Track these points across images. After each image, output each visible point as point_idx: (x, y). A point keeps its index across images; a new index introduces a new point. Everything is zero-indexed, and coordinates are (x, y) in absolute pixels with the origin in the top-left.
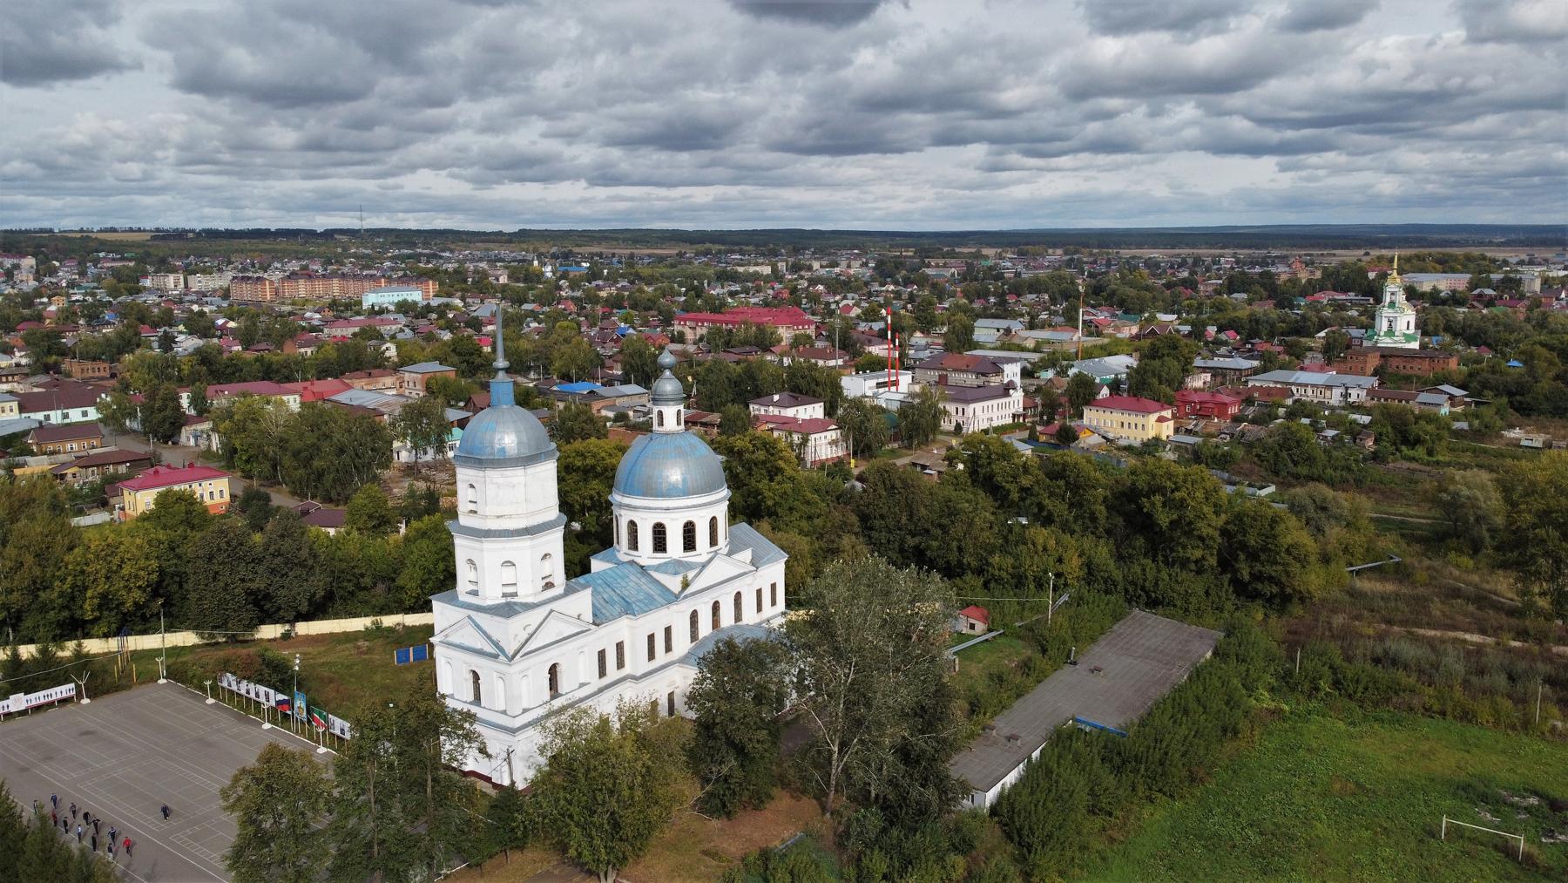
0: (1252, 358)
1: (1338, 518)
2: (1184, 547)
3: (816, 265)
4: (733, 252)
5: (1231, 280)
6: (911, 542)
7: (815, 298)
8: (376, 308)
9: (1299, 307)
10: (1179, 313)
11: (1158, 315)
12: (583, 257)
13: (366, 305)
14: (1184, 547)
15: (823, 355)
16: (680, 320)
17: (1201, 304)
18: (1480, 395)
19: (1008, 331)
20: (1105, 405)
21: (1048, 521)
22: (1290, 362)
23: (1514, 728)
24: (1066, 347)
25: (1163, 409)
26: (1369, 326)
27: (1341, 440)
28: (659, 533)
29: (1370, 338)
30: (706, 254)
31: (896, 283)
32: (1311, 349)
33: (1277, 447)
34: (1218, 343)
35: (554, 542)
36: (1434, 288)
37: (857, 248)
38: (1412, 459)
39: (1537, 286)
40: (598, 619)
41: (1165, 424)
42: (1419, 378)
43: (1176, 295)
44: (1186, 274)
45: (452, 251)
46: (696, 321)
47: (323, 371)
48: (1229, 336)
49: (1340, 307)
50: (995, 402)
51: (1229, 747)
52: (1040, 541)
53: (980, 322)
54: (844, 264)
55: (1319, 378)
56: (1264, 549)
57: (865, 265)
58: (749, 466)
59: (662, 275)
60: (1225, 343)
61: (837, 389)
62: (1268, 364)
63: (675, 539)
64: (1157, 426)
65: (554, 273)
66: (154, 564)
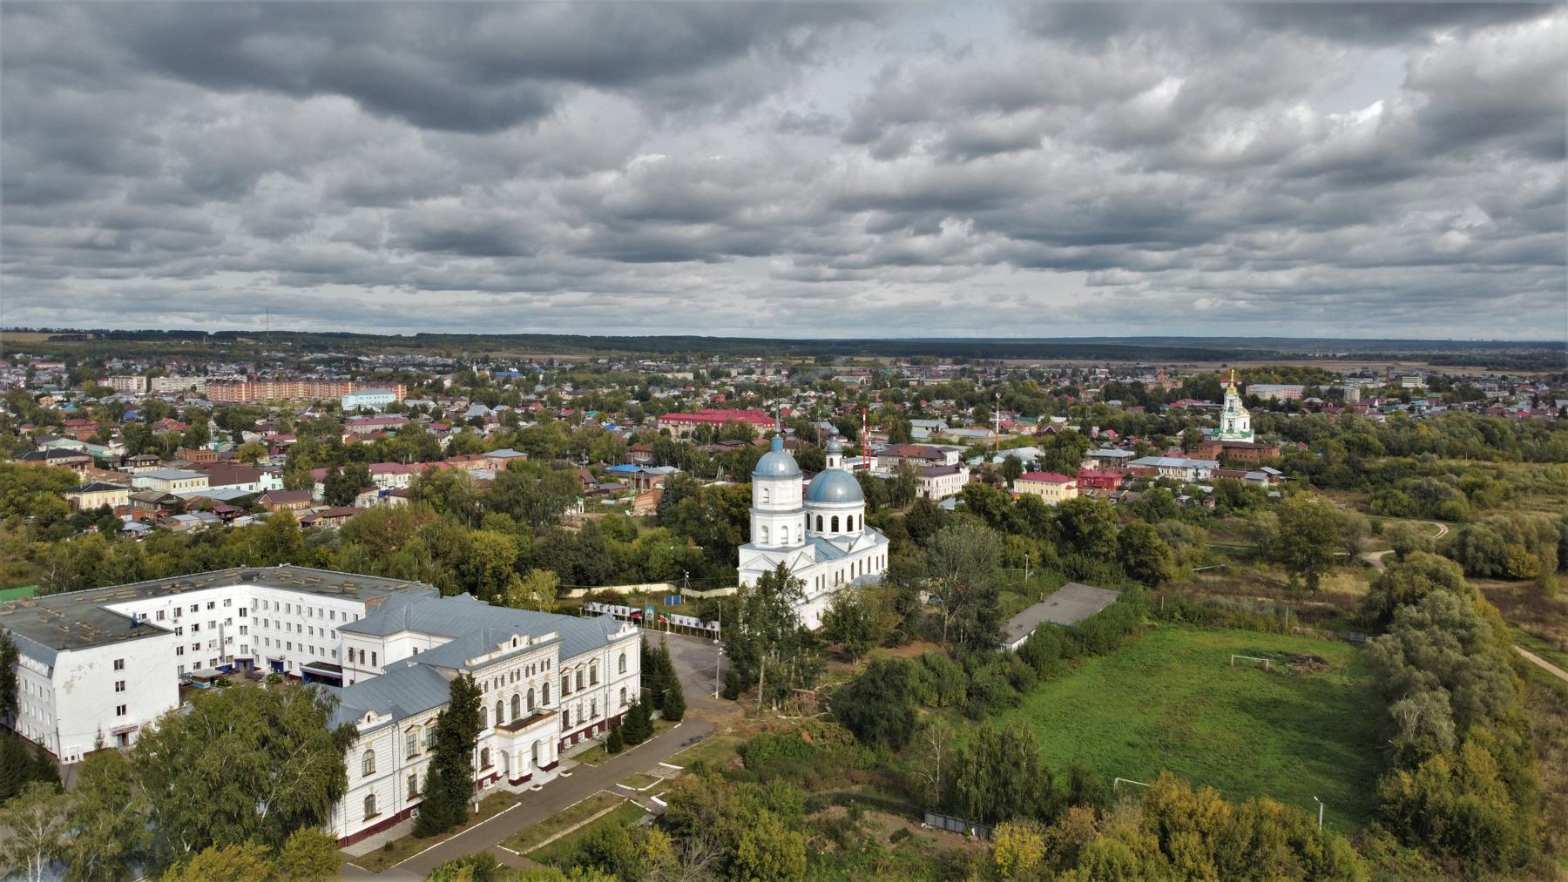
0: (1128, 449)
1: (1187, 541)
3: (734, 372)
5: (1107, 388)
9: (1164, 412)
17: (1083, 410)
18: (1290, 474)
19: (936, 430)
20: (1024, 478)
21: (1017, 532)
26: (1217, 426)
29: (1216, 435)
31: (816, 390)
32: (1173, 444)
34: (1101, 439)
38: (1241, 516)
39: (1357, 396)
43: (1063, 401)
44: (1067, 383)
46: (679, 420)
49: (1196, 411)
51: (1127, 638)
52: (1015, 542)
55: (1178, 462)
56: (1144, 546)
60: (1107, 440)
62: (1141, 452)
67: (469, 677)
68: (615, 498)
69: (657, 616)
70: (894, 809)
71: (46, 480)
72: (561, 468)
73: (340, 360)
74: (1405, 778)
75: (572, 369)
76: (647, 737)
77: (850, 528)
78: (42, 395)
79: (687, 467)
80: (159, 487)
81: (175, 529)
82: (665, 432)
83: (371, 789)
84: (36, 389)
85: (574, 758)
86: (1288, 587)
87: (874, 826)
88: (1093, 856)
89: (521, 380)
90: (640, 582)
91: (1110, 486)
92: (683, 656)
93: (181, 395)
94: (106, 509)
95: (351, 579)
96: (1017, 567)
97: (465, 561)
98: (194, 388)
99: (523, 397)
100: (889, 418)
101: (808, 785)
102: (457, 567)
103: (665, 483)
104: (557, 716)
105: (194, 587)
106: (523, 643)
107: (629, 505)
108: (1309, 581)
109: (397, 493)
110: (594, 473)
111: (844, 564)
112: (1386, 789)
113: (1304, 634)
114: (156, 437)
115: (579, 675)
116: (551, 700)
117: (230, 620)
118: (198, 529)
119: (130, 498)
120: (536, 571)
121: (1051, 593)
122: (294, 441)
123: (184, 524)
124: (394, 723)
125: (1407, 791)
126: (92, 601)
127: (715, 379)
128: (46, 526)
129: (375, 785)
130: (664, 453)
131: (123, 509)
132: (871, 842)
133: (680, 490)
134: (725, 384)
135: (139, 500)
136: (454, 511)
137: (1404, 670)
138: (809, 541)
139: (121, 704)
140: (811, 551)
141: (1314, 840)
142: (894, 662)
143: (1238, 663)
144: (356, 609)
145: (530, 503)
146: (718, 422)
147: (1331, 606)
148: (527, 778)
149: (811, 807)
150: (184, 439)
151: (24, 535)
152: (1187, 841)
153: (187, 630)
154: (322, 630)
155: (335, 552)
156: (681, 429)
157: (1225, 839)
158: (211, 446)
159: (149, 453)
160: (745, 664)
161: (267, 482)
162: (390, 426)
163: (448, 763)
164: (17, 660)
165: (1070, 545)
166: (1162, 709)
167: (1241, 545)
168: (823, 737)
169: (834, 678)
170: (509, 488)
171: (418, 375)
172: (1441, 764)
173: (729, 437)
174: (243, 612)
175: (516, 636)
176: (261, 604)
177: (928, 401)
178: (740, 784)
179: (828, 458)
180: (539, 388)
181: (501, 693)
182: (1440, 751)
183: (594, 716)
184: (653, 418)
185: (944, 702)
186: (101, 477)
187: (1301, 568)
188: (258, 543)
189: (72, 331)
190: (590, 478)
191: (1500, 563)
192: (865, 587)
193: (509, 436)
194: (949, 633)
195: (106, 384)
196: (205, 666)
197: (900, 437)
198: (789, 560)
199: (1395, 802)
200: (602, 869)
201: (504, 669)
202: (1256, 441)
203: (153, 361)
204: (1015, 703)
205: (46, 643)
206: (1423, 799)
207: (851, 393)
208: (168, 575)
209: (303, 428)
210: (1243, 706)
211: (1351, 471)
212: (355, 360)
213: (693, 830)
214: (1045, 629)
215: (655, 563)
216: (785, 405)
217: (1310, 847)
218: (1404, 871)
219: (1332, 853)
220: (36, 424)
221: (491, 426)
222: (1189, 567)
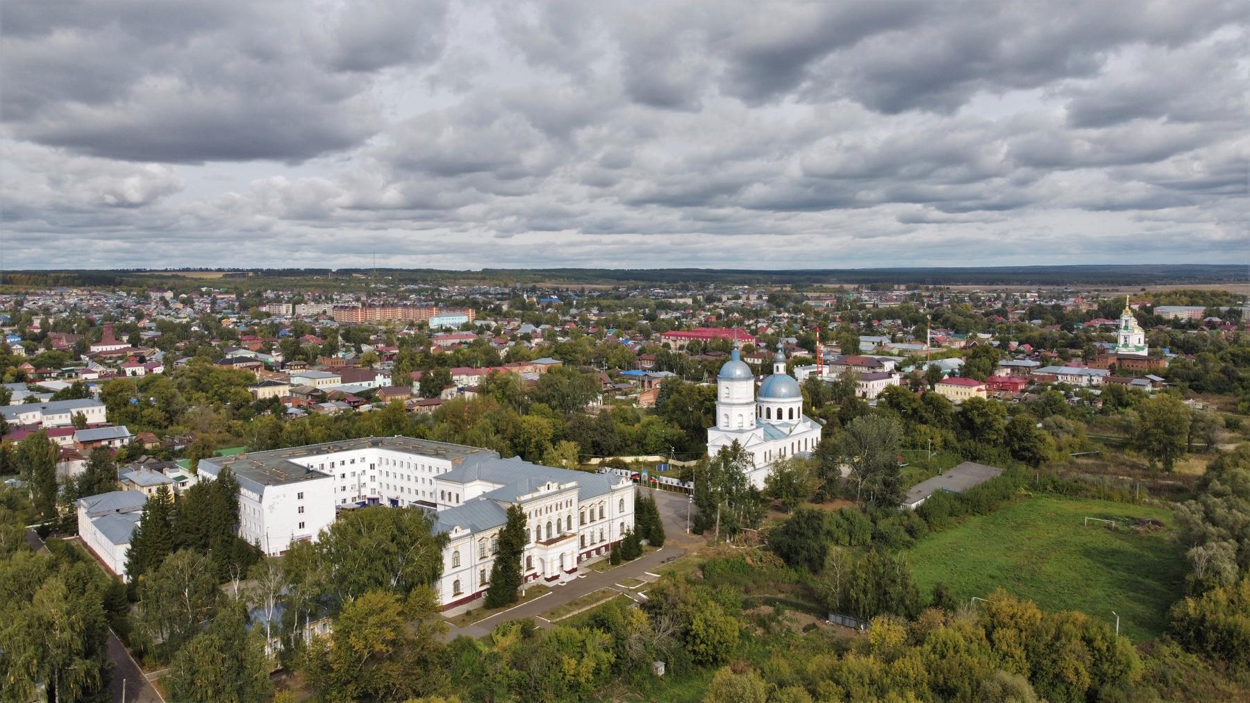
2: (988, 434)
3: (724, 298)
4: (654, 287)
10: (993, 333)
11: (978, 334)
14: (988, 434)
18: (1172, 381)
19: (880, 344)
20: (946, 382)
21: (925, 423)
22: (1058, 362)
23: (1128, 502)
24: (919, 353)
25: (980, 384)
27: (1083, 403)
29: (1113, 348)
31: (788, 312)
33: (1044, 405)
34: (1018, 352)
36: (1176, 316)
37: (746, 284)
42: (1136, 372)
44: (999, 305)
46: (677, 336)
48: (1026, 348)
51: (1005, 503)
56: (1025, 435)
60: (1022, 352)
62: (1045, 362)
64: (978, 392)
67: (519, 507)
68: (626, 394)
69: (650, 478)
70: (808, 610)
71: (236, 379)
72: (587, 372)
73: (426, 290)
74: (1191, 603)
75: (599, 296)
76: (638, 555)
77: (791, 417)
78: (223, 318)
79: (680, 373)
80: (309, 383)
82: (667, 346)
83: (458, 576)
84: (218, 313)
85: (587, 567)
86: (1148, 469)
87: (791, 620)
88: (934, 638)
89: (560, 305)
90: (638, 455)
91: (1015, 389)
92: (665, 505)
93: (316, 318)
94: (276, 399)
95: (442, 446)
96: (924, 449)
97: (516, 436)
98: (325, 312)
99: (560, 318)
100: (844, 334)
101: (747, 591)
102: (511, 440)
103: (661, 383)
104: (577, 537)
105: (341, 449)
106: (554, 487)
107: (636, 400)
108: (1165, 464)
109: (470, 389)
110: (610, 376)
111: (786, 443)
112: (1176, 611)
113: (1151, 504)
114: (302, 348)
115: (592, 512)
116: (573, 527)
117: (364, 471)
118: (336, 413)
119: (290, 391)
120: (563, 442)
121: (948, 469)
122: (397, 351)
123: (326, 409)
124: (473, 534)
125: (1191, 611)
126: (280, 457)
127: (710, 303)
128: (238, 409)
130: (664, 361)
131: (288, 399)
132: (789, 630)
133: (672, 389)
134: (717, 307)
135: (297, 393)
136: (510, 401)
137: (1202, 526)
138: (759, 425)
139: (301, 522)
140: (760, 432)
141: (1102, 638)
142: (813, 511)
143: (1091, 524)
144: (445, 465)
145: (564, 397)
146: (707, 338)
147: (1180, 483)
148: (557, 577)
149: (746, 605)
150: (322, 350)
151: (225, 415)
152: (1006, 636)
154: (423, 479)
155: (430, 429)
156: (679, 343)
157: (1036, 634)
158: (340, 355)
159: (299, 360)
160: (708, 511)
161: (380, 381)
162: (464, 341)
163: (506, 562)
164: (239, 491)
165: (968, 433)
166: (1021, 553)
167: (1116, 436)
168: (761, 561)
169: (770, 521)
170: (548, 386)
171: (484, 302)
172: (1220, 595)
173: (714, 350)
174: (372, 466)
175: (549, 483)
177: (880, 320)
178: (698, 587)
179: (775, 365)
180: (573, 311)
181: (540, 520)
182: (1222, 586)
183: (602, 540)
184: (658, 335)
185: (854, 543)
186: (269, 376)
187: (1158, 454)
188: (380, 421)
189: (238, 270)
190: (608, 380)
192: (797, 459)
193: (549, 348)
194: (862, 494)
195: (264, 309)
196: (349, 501)
197: (850, 349)
198: (742, 441)
199: (1182, 620)
200: (602, 631)
202: (1149, 354)
203: (296, 292)
204: (908, 546)
205: (257, 481)
206: (1202, 620)
207: (817, 314)
208: (324, 441)
209: (403, 342)
210: (1087, 553)
211: (1226, 378)
212: (437, 290)
213: (663, 611)
214: (939, 494)
215: (650, 440)
216: (762, 324)
217: (1098, 643)
218: (1181, 668)
219: (1115, 647)
220: (222, 339)
221: (537, 340)
222: (1067, 452)
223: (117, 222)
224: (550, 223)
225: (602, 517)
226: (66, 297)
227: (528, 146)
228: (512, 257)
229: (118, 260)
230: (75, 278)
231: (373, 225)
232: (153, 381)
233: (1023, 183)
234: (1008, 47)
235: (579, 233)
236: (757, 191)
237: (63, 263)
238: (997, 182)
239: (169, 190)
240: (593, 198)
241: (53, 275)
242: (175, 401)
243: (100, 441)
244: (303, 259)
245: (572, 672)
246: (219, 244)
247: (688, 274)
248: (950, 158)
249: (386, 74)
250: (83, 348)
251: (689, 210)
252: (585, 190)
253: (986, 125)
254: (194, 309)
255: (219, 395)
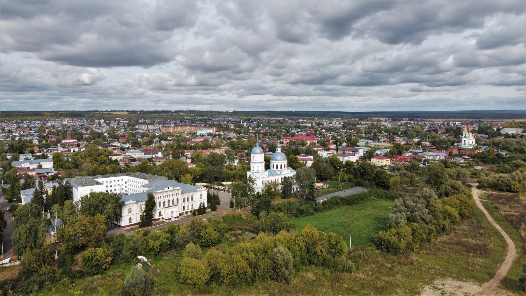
3: (325, 123)
4: (300, 119)
6: (319, 174)
7: (321, 133)
8: (202, 135)
12: (254, 120)
13: (198, 134)
15: (317, 147)
16: (282, 138)
25: (388, 158)
28: (277, 166)
30: (292, 120)
31: (347, 129)
35: (263, 164)
40: (269, 176)
41: (388, 162)
45: (215, 118)
46: (287, 139)
47: (203, 148)
50: (351, 157)
52: (341, 174)
53: (362, 140)
54: (333, 123)
57: (340, 123)
58: (292, 162)
59: (278, 126)
61: (316, 152)
63: (279, 167)
65: (247, 125)
66: (200, 172)
81: (131, 166)
94: (116, 160)
105: (115, 176)
119: (123, 157)
129: (131, 216)
144: (146, 182)
148: (170, 219)
153: (113, 186)
164: (73, 189)
175: (169, 187)
176: (129, 181)
179: (277, 149)
181: (165, 199)
191: (509, 187)
201: (164, 194)
220: (112, 138)
223: (84, 91)
224: (259, 92)
225: (192, 199)
226: (63, 121)
227: (242, 59)
228: (246, 106)
229: (89, 107)
230: (67, 114)
231: (187, 92)
232: (78, 154)
233: (462, 74)
234: (442, 15)
235: (272, 96)
236: (343, 78)
237: (66, 108)
238: (448, 74)
239: (100, 79)
240: (275, 81)
241: (60, 113)
242: (79, 160)
243: (44, 173)
244: (161, 106)
245: (152, 245)
246: (126, 100)
247: (319, 113)
248: (425, 65)
249: (176, 31)
250: (59, 141)
251: (317, 86)
252: (271, 78)
253: (437, 49)
254: (109, 127)
255: (95, 159)
